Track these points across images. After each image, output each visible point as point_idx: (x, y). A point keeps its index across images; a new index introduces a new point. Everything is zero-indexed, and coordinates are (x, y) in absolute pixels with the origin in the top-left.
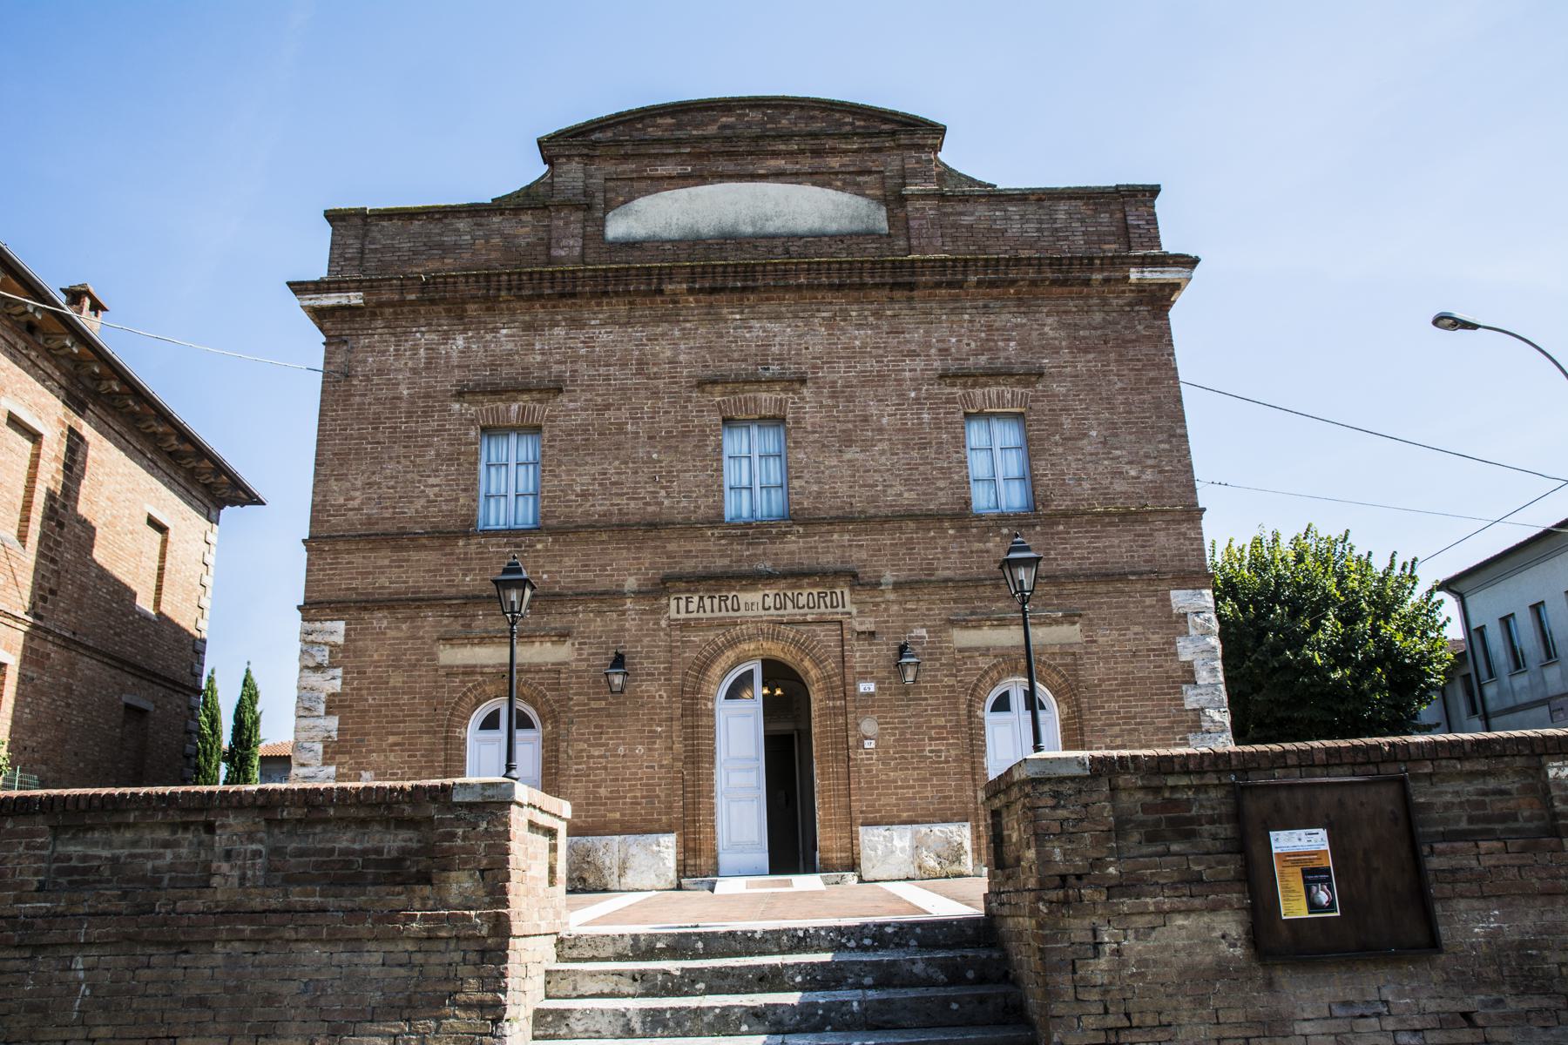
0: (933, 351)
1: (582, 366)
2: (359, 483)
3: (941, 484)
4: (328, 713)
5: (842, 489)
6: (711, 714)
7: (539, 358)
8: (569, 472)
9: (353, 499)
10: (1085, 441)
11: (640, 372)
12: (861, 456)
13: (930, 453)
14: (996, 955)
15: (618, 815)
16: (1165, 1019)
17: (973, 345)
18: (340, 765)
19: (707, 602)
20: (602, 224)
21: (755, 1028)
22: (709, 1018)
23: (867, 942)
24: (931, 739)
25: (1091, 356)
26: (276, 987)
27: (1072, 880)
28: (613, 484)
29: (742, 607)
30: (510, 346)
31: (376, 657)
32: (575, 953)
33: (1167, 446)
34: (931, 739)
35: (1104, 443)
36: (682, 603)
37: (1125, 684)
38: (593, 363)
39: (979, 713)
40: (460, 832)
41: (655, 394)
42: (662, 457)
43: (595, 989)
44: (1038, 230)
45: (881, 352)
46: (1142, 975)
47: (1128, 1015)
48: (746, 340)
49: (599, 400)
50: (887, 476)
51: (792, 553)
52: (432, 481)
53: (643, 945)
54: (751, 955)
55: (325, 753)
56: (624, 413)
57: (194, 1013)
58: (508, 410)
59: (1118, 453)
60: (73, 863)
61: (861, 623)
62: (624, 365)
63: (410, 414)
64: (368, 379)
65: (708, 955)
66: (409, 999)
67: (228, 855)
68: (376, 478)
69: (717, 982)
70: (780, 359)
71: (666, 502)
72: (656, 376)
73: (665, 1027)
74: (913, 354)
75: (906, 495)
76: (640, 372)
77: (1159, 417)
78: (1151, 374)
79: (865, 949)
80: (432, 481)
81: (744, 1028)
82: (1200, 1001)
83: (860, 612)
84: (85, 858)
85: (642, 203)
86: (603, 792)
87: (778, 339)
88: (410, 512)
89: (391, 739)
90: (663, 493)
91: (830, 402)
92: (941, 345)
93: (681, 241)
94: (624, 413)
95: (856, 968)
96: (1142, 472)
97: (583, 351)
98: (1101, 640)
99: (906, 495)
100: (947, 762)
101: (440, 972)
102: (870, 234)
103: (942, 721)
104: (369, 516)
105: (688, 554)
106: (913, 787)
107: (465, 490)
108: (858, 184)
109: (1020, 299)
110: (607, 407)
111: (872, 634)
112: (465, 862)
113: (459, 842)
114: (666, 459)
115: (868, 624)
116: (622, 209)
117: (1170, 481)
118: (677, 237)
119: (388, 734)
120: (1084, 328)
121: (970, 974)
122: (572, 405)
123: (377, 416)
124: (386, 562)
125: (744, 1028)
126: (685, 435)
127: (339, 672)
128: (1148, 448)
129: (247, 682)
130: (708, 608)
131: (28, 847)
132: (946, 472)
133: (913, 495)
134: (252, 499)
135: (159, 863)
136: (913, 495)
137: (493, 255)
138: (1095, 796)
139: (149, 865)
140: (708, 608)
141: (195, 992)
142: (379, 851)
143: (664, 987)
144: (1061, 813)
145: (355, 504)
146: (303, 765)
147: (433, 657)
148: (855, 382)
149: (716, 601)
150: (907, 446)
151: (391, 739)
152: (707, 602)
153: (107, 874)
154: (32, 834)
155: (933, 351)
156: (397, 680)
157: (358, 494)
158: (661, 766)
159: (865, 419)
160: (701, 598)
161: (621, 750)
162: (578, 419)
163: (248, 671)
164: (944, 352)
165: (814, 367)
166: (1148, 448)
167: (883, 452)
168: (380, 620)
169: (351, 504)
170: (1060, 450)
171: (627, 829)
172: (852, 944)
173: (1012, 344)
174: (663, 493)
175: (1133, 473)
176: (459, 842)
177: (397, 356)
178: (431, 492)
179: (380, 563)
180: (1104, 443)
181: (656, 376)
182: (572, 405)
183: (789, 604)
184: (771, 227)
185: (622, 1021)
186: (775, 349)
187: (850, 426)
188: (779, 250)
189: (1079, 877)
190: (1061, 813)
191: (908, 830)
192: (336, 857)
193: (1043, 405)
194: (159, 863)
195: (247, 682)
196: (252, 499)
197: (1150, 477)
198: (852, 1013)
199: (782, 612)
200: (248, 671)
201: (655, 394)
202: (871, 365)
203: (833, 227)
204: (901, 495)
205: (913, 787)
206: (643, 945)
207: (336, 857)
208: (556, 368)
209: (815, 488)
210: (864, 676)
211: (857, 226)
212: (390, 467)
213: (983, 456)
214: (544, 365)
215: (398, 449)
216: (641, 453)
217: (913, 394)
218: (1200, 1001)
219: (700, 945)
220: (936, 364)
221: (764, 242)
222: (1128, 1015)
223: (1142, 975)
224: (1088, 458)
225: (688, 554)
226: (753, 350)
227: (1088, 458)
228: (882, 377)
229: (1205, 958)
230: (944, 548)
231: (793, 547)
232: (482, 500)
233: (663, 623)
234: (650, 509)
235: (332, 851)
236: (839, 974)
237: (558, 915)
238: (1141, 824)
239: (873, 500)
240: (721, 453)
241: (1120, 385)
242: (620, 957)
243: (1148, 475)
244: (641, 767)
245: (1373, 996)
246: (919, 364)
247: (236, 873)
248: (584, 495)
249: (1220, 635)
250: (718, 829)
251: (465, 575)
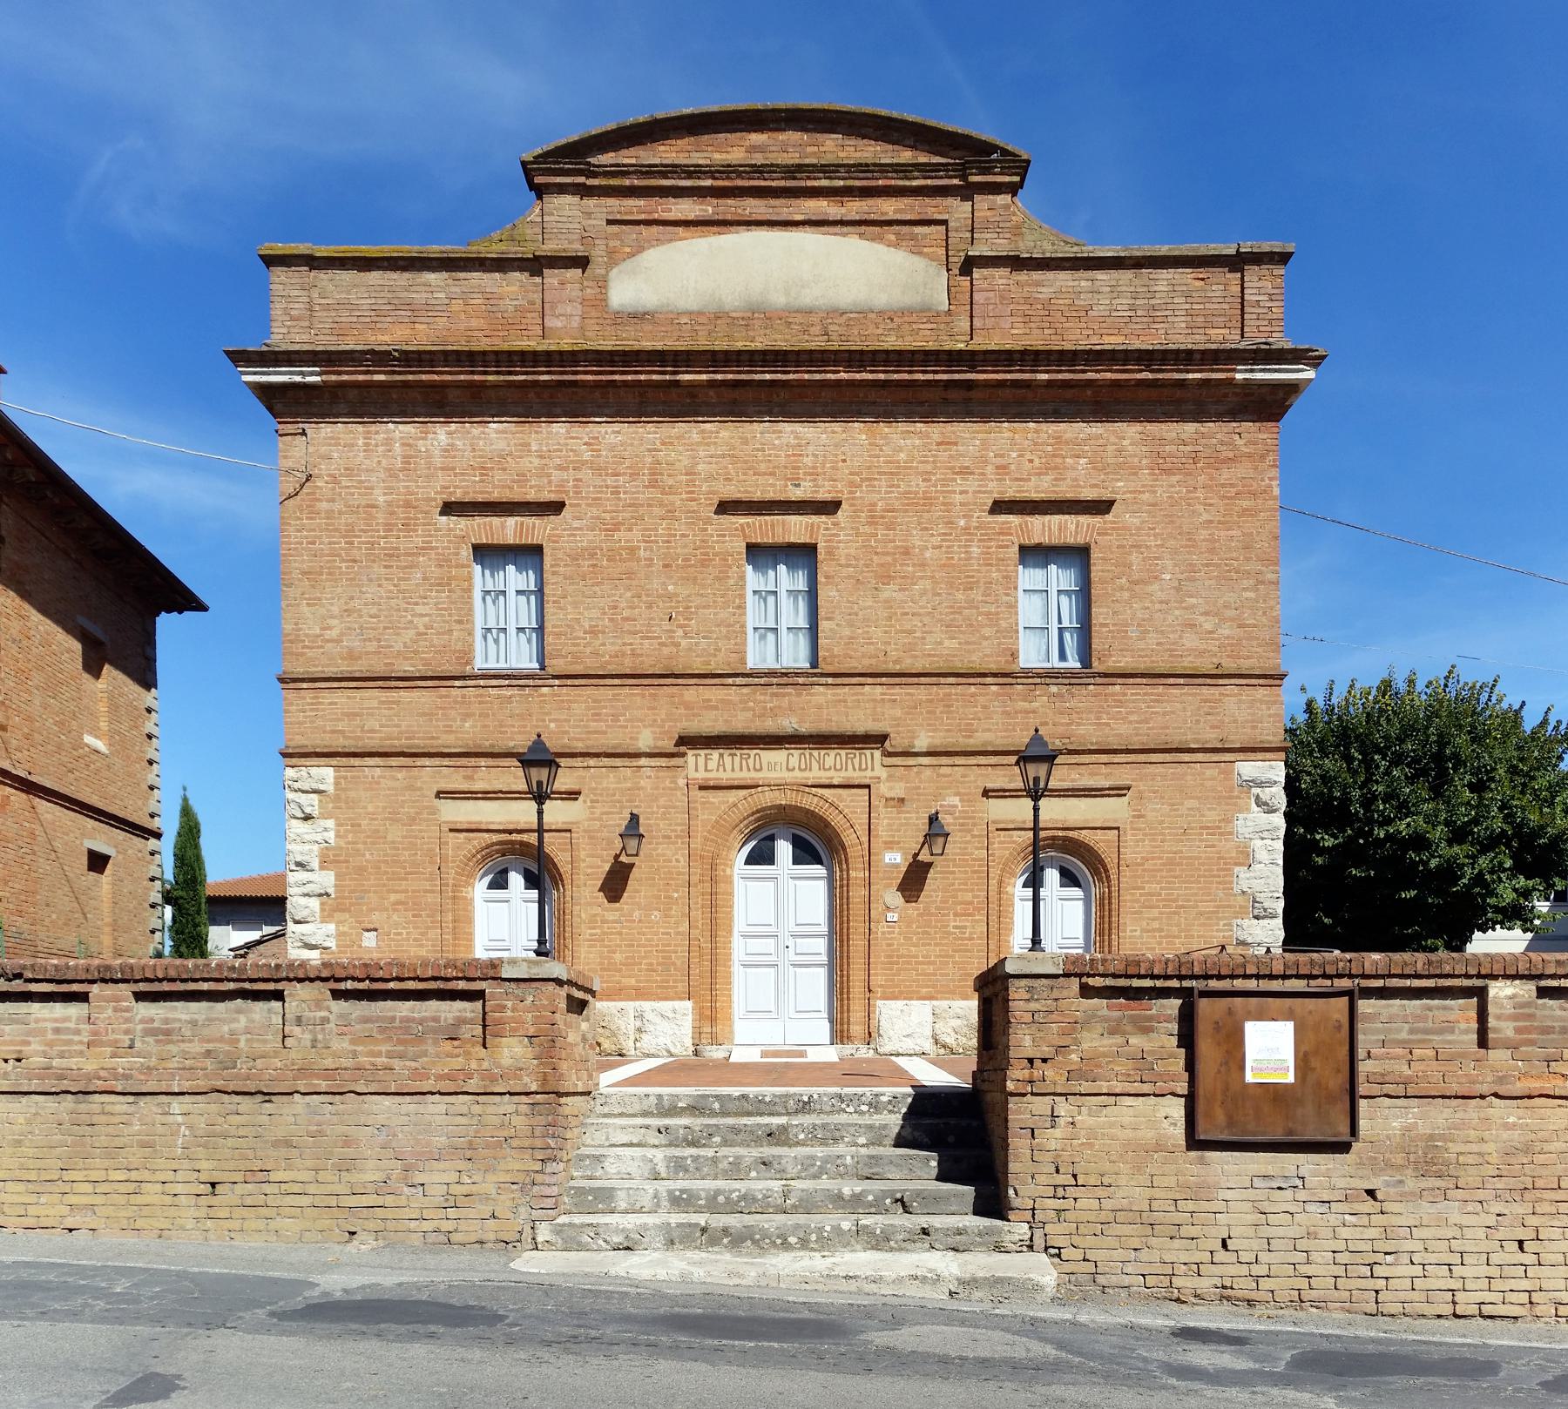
0: (989, 468)
1: (586, 474)
2: (335, 610)
3: (987, 632)
4: (322, 868)
5: (877, 633)
6: (729, 880)
7: (536, 462)
8: (575, 604)
9: (330, 628)
10: (1156, 587)
11: (653, 484)
12: (899, 596)
13: (977, 595)
14: (975, 1124)
15: (633, 981)
16: (1106, 1181)
17: (1037, 461)
18: (338, 923)
19: (728, 760)
20: (603, 283)
21: (763, 1174)
22: (724, 1165)
23: (865, 1108)
24: (956, 915)
25: (1174, 479)
26: (352, 1131)
27: (1037, 1063)
28: (627, 619)
29: (765, 766)
30: (501, 445)
31: (370, 809)
32: (606, 1110)
33: (1251, 595)
34: (956, 915)
35: (1178, 589)
36: (701, 760)
37: (1171, 862)
38: (598, 470)
39: (1009, 889)
40: (509, 1004)
41: (671, 514)
42: (680, 590)
43: (625, 1139)
44: (1132, 308)
45: (929, 467)
46: (1091, 1145)
47: (1075, 1176)
48: (774, 447)
49: (607, 516)
50: (926, 620)
51: (820, 707)
52: (419, 609)
53: (666, 1103)
54: (761, 1115)
55: (322, 910)
56: (636, 534)
57: (283, 1152)
58: (503, 526)
59: (1194, 601)
60: (156, 1025)
61: (891, 788)
62: (634, 475)
63: (389, 527)
64: (334, 480)
65: (725, 1113)
66: (470, 1143)
67: (299, 1021)
68: (356, 604)
69: (731, 1136)
70: (814, 474)
71: (684, 643)
72: (671, 491)
73: (687, 1171)
74: (965, 472)
75: (947, 643)
76: (653, 484)
77: (1248, 559)
78: (1246, 504)
79: (862, 1113)
80: (419, 609)
81: (754, 1174)
82: (1138, 1169)
83: (890, 777)
84: (166, 1021)
85: (651, 256)
86: (618, 957)
87: (811, 448)
88: (399, 646)
89: (393, 897)
90: (680, 632)
91: (867, 529)
92: (999, 461)
93: (700, 313)
94: (636, 534)
95: (852, 1130)
96: (1218, 625)
97: (587, 456)
98: (1151, 815)
99: (947, 643)
100: (971, 939)
101: (496, 1120)
102: (925, 312)
103: (969, 896)
104: (351, 650)
105: (708, 706)
106: (933, 963)
107: (460, 622)
108: (913, 238)
109: (1097, 403)
110: (616, 527)
111: (902, 800)
112: (515, 1030)
113: (509, 1013)
114: (684, 592)
115: (898, 790)
116: (628, 265)
117: (1250, 638)
118: (695, 307)
119: (389, 891)
120: (1172, 442)
121: (951, 1139)
122: (576, 524)
123: (350, 529)
124: (375, 704)
125: (754, 1174)
126: (704, 563)
127: (330, 823)
128: (1230, 597)
129: (187, 812)
130: (728, 767)
131: (115, 1010)
132: (993, 618)
133: (954, 644)
134: (202, 608)
135: (234, 1026)
136: (954, 644)
137: (474, 323)
138: (1065, 993)
139: (226, 1028)
140: (728, 767)
141: (280, 1133)
142: (436, 1019)
143: (685, 1140)
144: (1033, 1006)
145: (334, 633)
146: (297, 922)
147: (434, 811)
148: (897, 505)
149: (737, 759)
150: (951, 585)
151: (393, 897)
152: (728, 760)
153: (188, 1033)
154: (117, 1000)
155: (989, 468)
156: (395, 833)
157: (334, 622)
158: (678, 933)
159: (906, 552)
160: (721, 755)
161: (636, 914)
162: (585, 540)
163: (185, 799)
164: (1002, 469)
165: (852, 484)
166: (1230, 597)
167: (924, 593)
168: (372, 769)
169: (328, 634)
170: (1126, 595)
171: (640, 994)
172: (851, 1109)
173: (1083, 461)
174: (680, 632)
175: (1208, 626)
176: (509, 1013)
177: (367, 449)
178: (420, 623)
179: (366, 704)
180: (1178, 589)
181: (671, 491)
182: (576, 524)
183: (815, 765)
184: (808, 298)
185: (650, 1165)
186: (808, 461)
187: (889, 559)
188: (816, 330)
189: (1044, 1061)
190: (1033, 1006)
191: (927, 1006)
192: (397, 1024)
193: (1112, 539)
194: (234, 1026)
195: (187, 812)
196: (202, 608)
197: (1227, 632)
198: (845, 1166)
199: (807, 774)
200: (185, 799)
201: (671, 514)
202: (917, 484)
203: (881, 300)
204: (941, 643)
205: (933, 963)
206: (666, 1103)
207: (397, 1024)
208: (556, 475)
209: (847, 632)
210: (890, 845)
211: (911, 299)
212: (371, 591)
213: (1037, 600)
214: (542, 472)
215: (377, 569)
216: (656, 584)
217: (962, 523)
218: (1138, 1169)
219: (717, 1106)
220: (992, 485)
221: (799, 318)
222: (1075, 1176)
223: (1091, 1145)
224: (1158, 606)
225: (708, 706)
226: (783, 460)
227: (1158, 606)
228: (928, 501)
229: (1148, 1135)
230: (985, 707)
231: (821, 699)
232: (478, 634)
233: (682, 782)
234: (666, 651)
235: (393, 1019)
236: (837, 1134)
237: (590, 1077)
238: (1105, 1019)
239: (909, 649)
240: (743, 587)
241: (1205, 517)
242: (645, 1114)
243: (1225, 631)
244: (656, 934)
245: (1292, 1171)
246: (972, 484)
247: (308, 1036)
248: (593, 632)
249: (1285, 814)
250: (735, 998)
251: (463, 720)
